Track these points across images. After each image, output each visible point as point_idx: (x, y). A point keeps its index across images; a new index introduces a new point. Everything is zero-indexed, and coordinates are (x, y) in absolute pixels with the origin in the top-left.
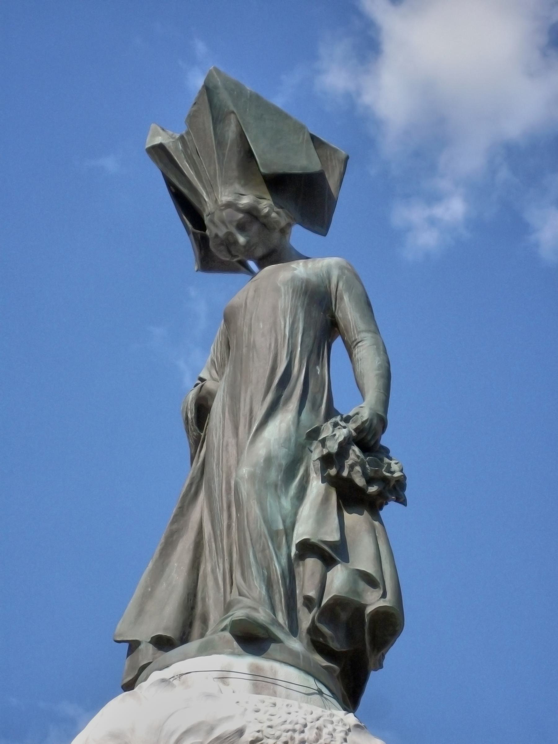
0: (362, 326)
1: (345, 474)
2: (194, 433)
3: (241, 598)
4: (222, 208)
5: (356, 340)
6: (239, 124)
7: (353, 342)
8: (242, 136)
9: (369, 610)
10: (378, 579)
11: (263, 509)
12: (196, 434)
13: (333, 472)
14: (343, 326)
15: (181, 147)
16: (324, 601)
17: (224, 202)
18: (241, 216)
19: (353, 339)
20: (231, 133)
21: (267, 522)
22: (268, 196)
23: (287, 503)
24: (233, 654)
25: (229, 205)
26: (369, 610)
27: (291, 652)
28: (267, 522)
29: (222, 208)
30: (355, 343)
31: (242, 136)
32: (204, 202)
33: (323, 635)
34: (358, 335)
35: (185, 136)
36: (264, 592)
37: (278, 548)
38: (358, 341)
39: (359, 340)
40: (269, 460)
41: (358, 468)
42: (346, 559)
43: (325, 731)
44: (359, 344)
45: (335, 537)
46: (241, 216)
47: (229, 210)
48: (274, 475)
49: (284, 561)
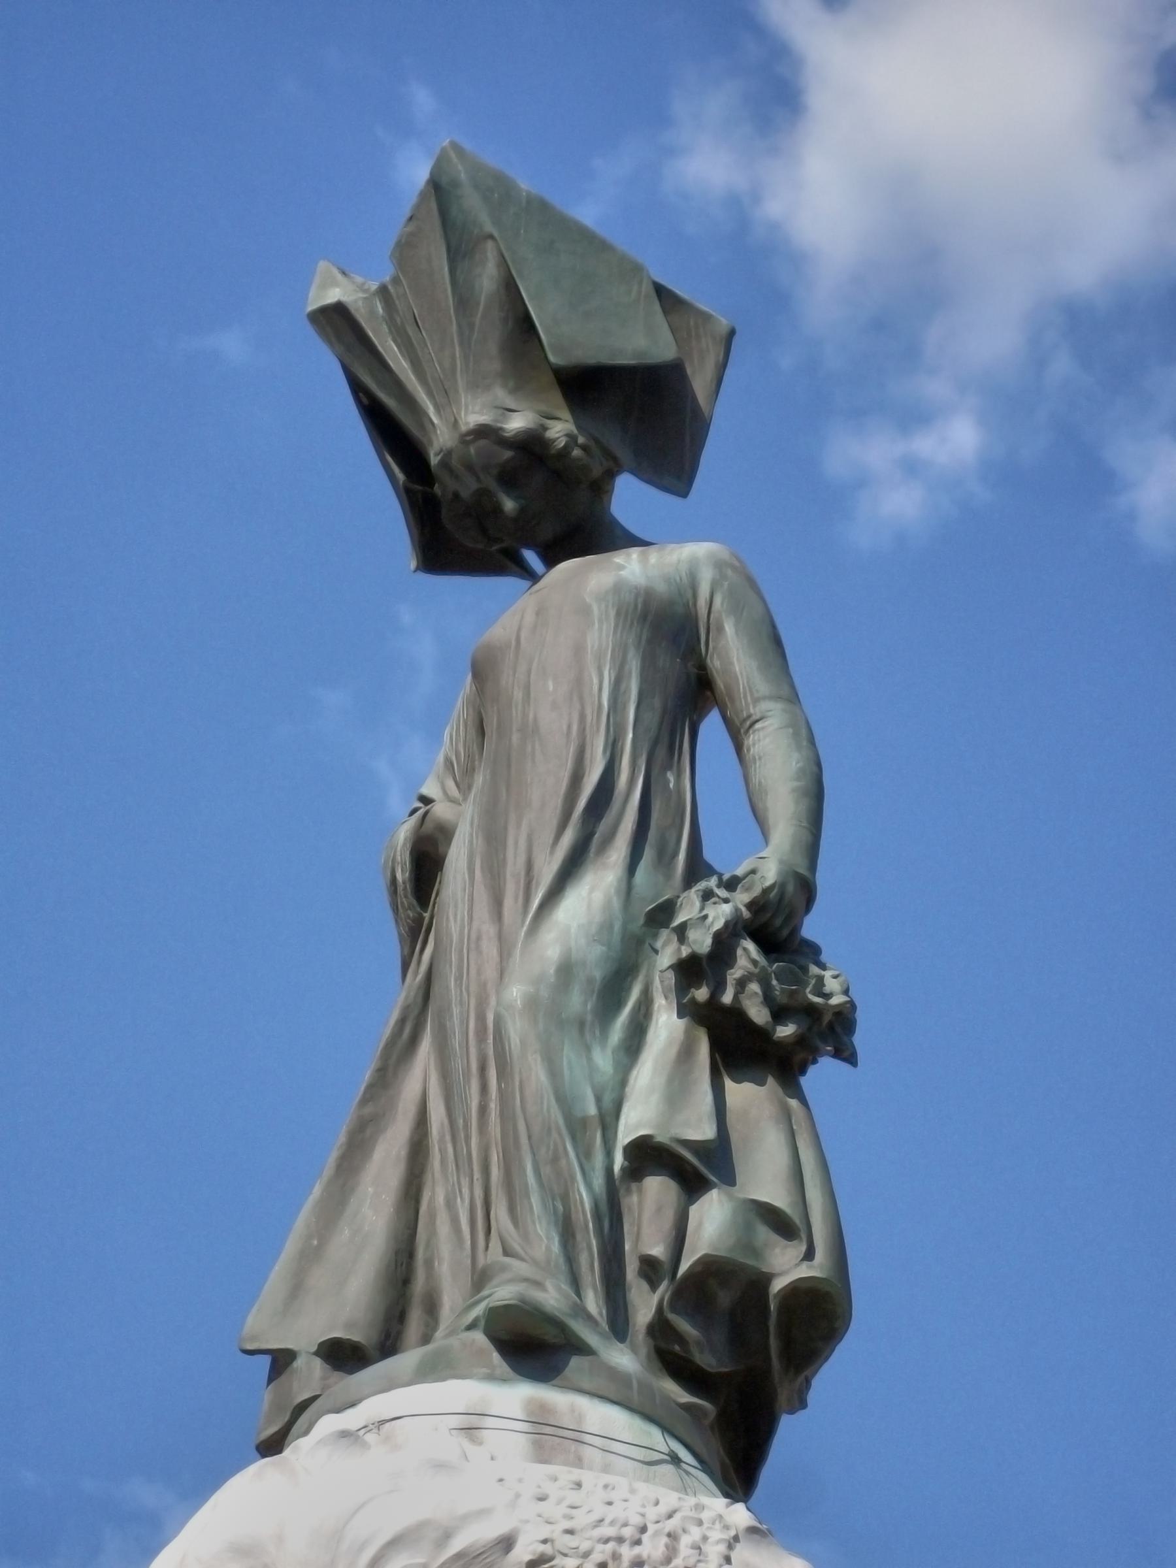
0: (762, 687)
1: (727, 998)
2: (409, 912)
3: (508, 1260)
4: (468, 438)
5: (749, 716)
6: (503, 262)
7: (745, 720)
8: (510, 287)
9: (778, 1285)
10: (796, 1218)
11: (554, 1073)
12: (413, 916)
13: (702, 994)
14: (722, 687)
15: (381, 310)
16: (684, 1267)
17: (472, 425)
18: (508, 454)
19: (745, 715)
20: (487, 279)
21: (563, 1100)
22: (566, 414)
23: (604, 1060)
24: (491, 1378)
25: (482, 432)
26: (778, 1285)
27: (614, 1375)
28: (563, 1100)
29: (468, 438)
30: (748, 723)
31: (510, 287)
32: (431, 426)
33: (680, 1338)
34: (754, 707)
35: (390, 287)
36: (556, 1247)
37: (585, 1155)
38: (754, 718)
39: (757, 717)
40: (566, 970)
41: (754, 987)
42: (729, 1178)
43: (685, 1541)
44: (758, 726)
45: (705, 1131)
46: (508, 454)
47: (482, 443)
48: (578, 1002)
49: (599, 1181)
